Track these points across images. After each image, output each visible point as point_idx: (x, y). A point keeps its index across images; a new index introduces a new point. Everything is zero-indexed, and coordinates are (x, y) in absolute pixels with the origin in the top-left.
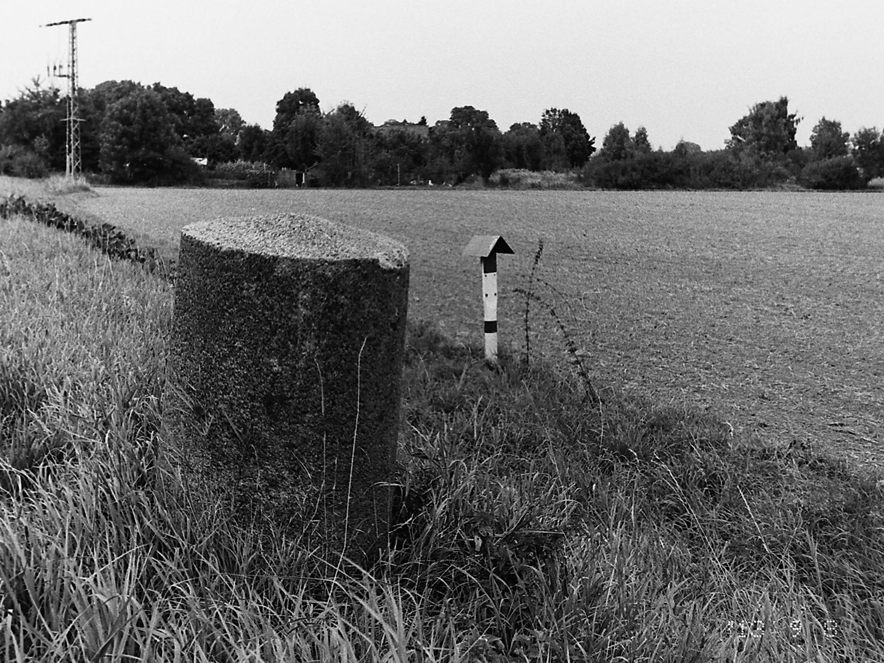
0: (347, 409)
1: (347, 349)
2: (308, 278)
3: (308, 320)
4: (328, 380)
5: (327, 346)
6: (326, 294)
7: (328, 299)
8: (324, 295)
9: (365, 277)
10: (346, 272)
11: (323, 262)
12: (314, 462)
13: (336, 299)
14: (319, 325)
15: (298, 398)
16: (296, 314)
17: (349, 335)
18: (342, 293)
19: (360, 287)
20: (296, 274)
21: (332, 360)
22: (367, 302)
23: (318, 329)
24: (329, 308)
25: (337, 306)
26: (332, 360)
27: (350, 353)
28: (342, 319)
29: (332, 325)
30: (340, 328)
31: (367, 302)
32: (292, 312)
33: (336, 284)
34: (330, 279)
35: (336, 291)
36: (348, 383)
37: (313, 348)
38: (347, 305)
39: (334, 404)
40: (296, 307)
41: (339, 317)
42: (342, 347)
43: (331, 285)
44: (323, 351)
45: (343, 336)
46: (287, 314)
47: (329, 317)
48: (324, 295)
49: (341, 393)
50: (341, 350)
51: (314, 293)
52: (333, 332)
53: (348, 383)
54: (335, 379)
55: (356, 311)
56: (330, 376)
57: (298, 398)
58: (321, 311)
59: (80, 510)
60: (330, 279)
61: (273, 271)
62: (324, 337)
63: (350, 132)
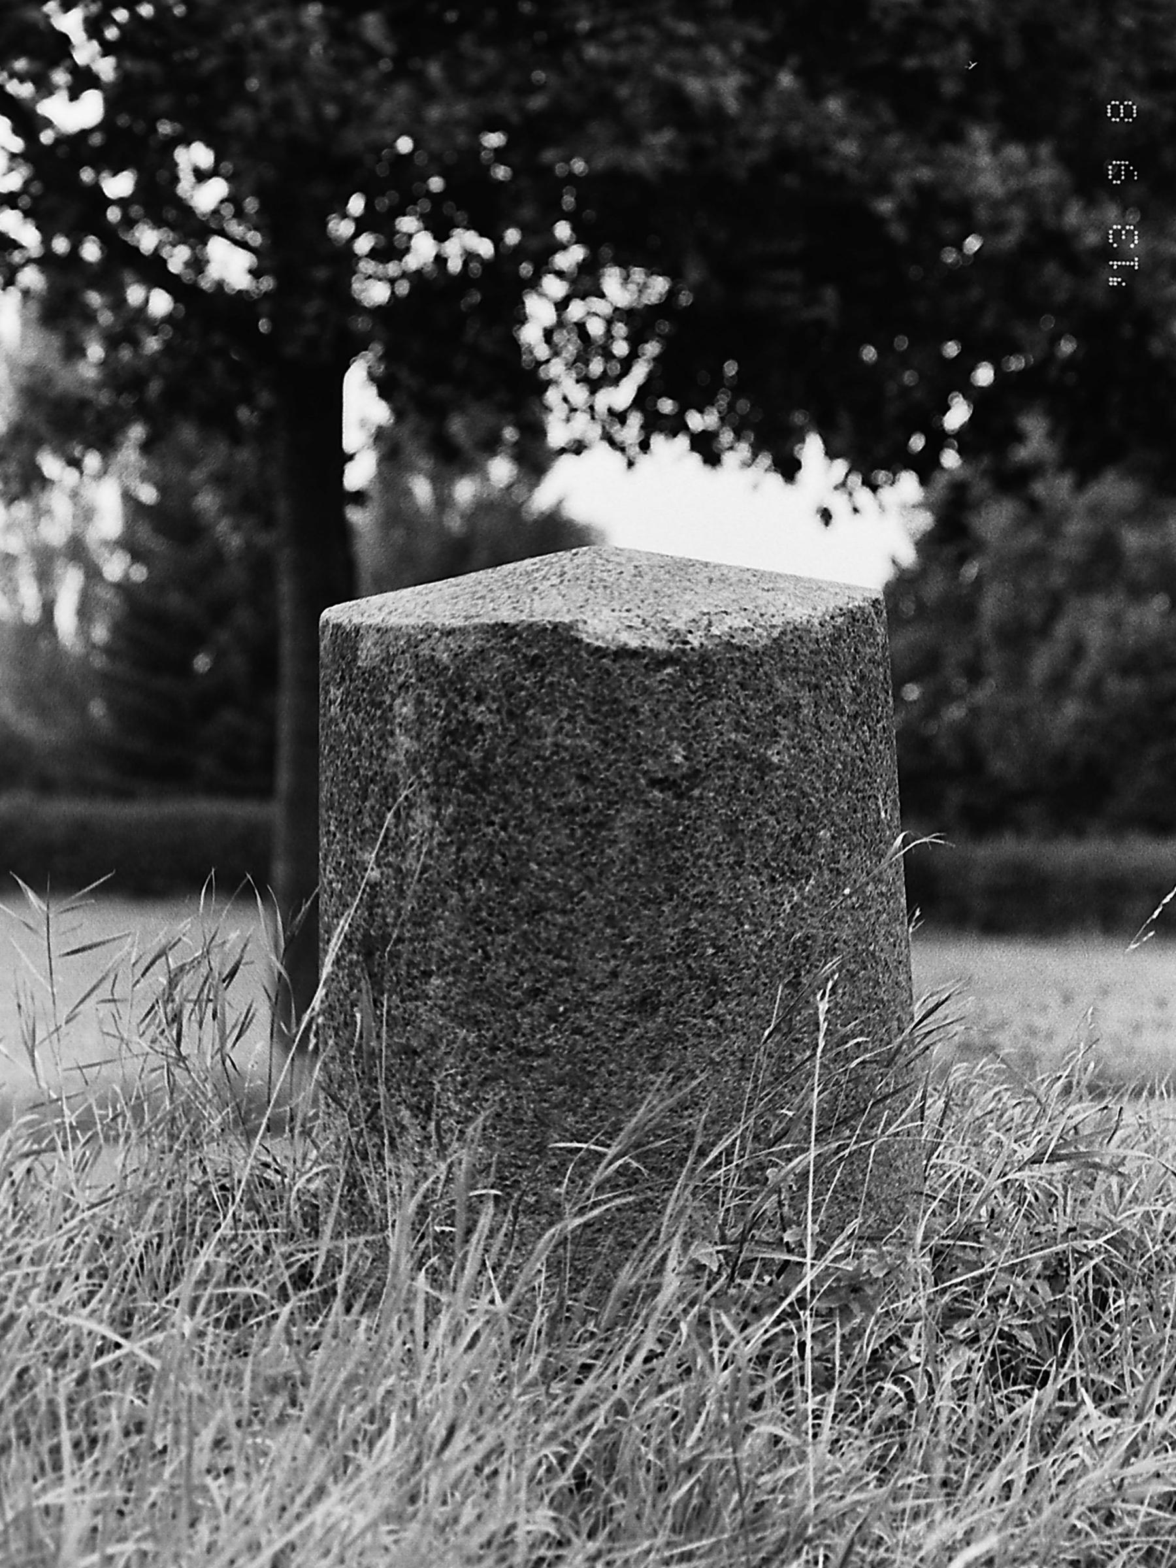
0: (522, 973)
1: (504, 827)
2: (405, 670)
3: (414, 762)
4: (466, 901)
5: (455, 821)
6: (443, 702)
7: (447, 714)
8: (438, 705)
9: (534, 663)
10: (481, 652)
11: (428, 631)
12: (457, 1093)
13: (465, 713)
14: (434, 771)
15: (411, 940)
16: (394, 749)
17: (506, 797)
18: (479, 699)
19: (522, 688)
20: (388, 660)
21: (471, 854)
22: (549, 724)
23: (435, 782)
24: (451, 733)
25: (469, 731)
26: (471, 854)
27: (512, 840)
28: (484, 758)
29: (462, 773)
30: (480, 782)
31: (549, 724)
32: (388, 746)
33: (461, 679)
34: (447, 668)
35: (463, 695)
36: (515, 909)
37: (428, 823)
38: (493, 727)
39: (487, 957)
40: (392, 733)
41: (475, 755)
42: (492, 823)
43: (451, 682)
44: (449, 832)
45: (489, 799)
46: (379, 749)
47: (453, 756)
48: (438, 705)
49: (500, 931)
50: (490, 830)
51: (419, 701)
52: (466, 789)
53: (515, 909)
54: (483, 899)
55: (515, 742)
56: (470, 892)
57: (411, 940)
58: (435, 740)
59: (681, 1202)
60: (447, 668)
61: (355, 658)
62: (449, 801)
63: (727, 437)
